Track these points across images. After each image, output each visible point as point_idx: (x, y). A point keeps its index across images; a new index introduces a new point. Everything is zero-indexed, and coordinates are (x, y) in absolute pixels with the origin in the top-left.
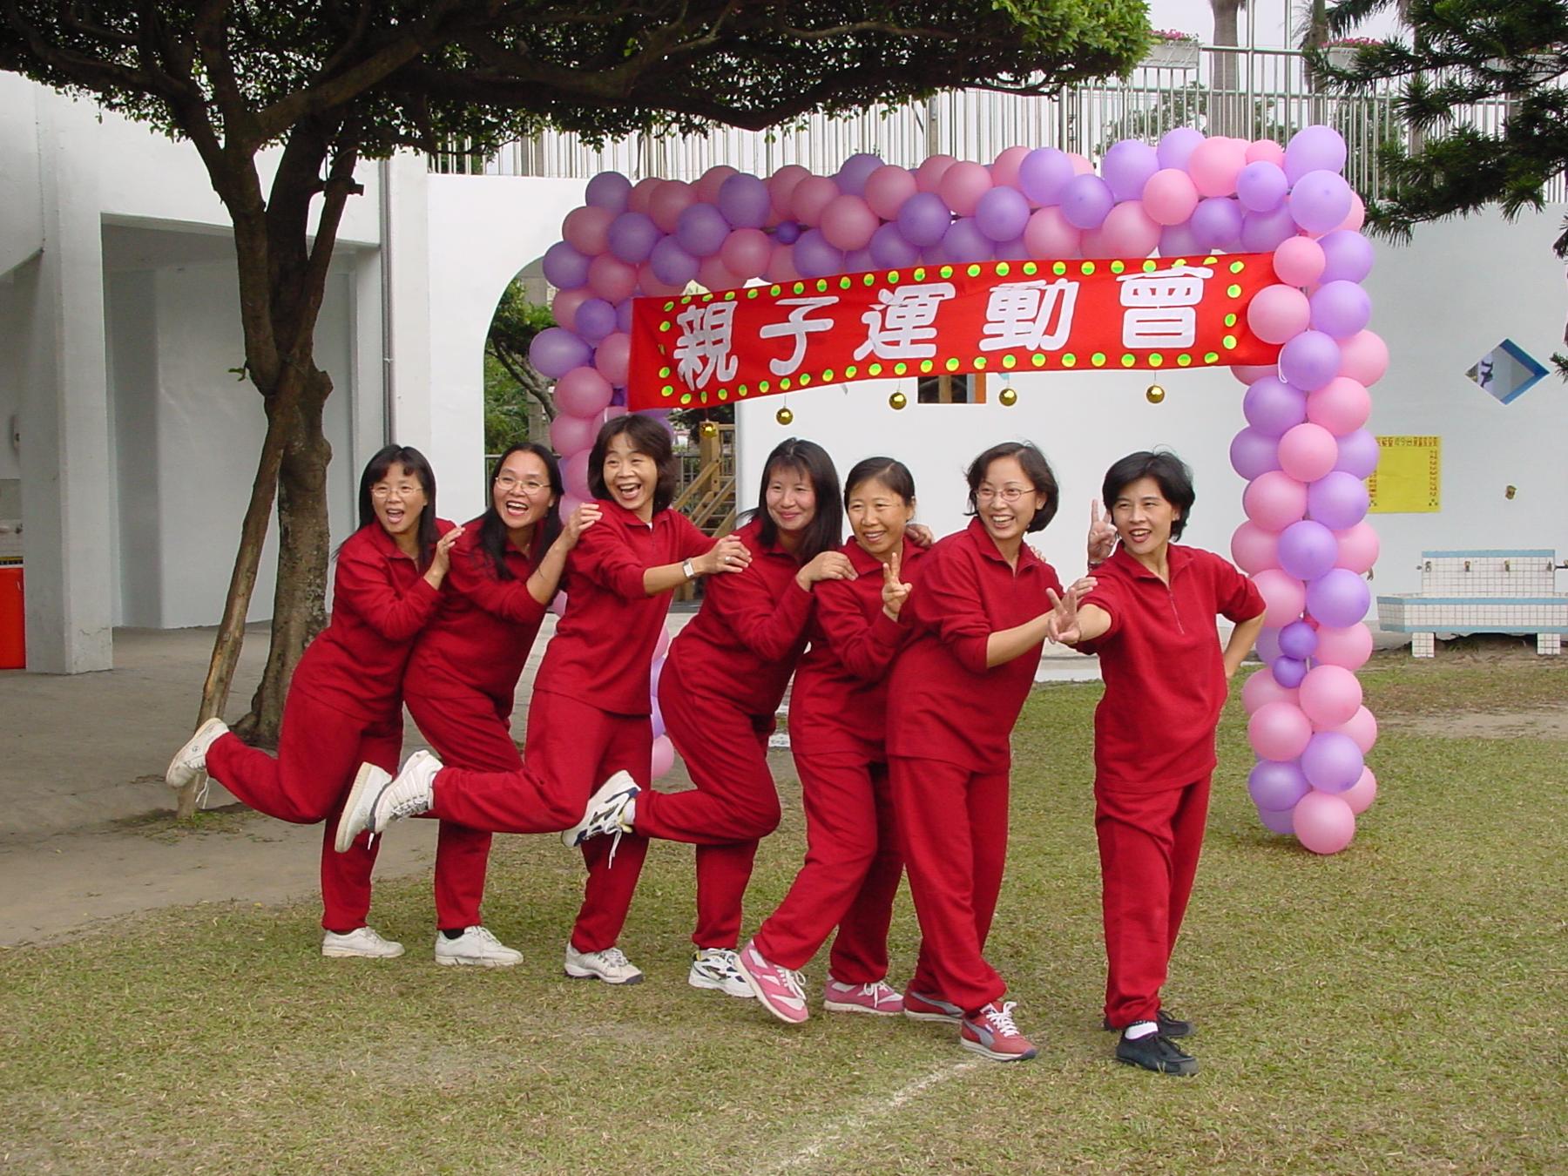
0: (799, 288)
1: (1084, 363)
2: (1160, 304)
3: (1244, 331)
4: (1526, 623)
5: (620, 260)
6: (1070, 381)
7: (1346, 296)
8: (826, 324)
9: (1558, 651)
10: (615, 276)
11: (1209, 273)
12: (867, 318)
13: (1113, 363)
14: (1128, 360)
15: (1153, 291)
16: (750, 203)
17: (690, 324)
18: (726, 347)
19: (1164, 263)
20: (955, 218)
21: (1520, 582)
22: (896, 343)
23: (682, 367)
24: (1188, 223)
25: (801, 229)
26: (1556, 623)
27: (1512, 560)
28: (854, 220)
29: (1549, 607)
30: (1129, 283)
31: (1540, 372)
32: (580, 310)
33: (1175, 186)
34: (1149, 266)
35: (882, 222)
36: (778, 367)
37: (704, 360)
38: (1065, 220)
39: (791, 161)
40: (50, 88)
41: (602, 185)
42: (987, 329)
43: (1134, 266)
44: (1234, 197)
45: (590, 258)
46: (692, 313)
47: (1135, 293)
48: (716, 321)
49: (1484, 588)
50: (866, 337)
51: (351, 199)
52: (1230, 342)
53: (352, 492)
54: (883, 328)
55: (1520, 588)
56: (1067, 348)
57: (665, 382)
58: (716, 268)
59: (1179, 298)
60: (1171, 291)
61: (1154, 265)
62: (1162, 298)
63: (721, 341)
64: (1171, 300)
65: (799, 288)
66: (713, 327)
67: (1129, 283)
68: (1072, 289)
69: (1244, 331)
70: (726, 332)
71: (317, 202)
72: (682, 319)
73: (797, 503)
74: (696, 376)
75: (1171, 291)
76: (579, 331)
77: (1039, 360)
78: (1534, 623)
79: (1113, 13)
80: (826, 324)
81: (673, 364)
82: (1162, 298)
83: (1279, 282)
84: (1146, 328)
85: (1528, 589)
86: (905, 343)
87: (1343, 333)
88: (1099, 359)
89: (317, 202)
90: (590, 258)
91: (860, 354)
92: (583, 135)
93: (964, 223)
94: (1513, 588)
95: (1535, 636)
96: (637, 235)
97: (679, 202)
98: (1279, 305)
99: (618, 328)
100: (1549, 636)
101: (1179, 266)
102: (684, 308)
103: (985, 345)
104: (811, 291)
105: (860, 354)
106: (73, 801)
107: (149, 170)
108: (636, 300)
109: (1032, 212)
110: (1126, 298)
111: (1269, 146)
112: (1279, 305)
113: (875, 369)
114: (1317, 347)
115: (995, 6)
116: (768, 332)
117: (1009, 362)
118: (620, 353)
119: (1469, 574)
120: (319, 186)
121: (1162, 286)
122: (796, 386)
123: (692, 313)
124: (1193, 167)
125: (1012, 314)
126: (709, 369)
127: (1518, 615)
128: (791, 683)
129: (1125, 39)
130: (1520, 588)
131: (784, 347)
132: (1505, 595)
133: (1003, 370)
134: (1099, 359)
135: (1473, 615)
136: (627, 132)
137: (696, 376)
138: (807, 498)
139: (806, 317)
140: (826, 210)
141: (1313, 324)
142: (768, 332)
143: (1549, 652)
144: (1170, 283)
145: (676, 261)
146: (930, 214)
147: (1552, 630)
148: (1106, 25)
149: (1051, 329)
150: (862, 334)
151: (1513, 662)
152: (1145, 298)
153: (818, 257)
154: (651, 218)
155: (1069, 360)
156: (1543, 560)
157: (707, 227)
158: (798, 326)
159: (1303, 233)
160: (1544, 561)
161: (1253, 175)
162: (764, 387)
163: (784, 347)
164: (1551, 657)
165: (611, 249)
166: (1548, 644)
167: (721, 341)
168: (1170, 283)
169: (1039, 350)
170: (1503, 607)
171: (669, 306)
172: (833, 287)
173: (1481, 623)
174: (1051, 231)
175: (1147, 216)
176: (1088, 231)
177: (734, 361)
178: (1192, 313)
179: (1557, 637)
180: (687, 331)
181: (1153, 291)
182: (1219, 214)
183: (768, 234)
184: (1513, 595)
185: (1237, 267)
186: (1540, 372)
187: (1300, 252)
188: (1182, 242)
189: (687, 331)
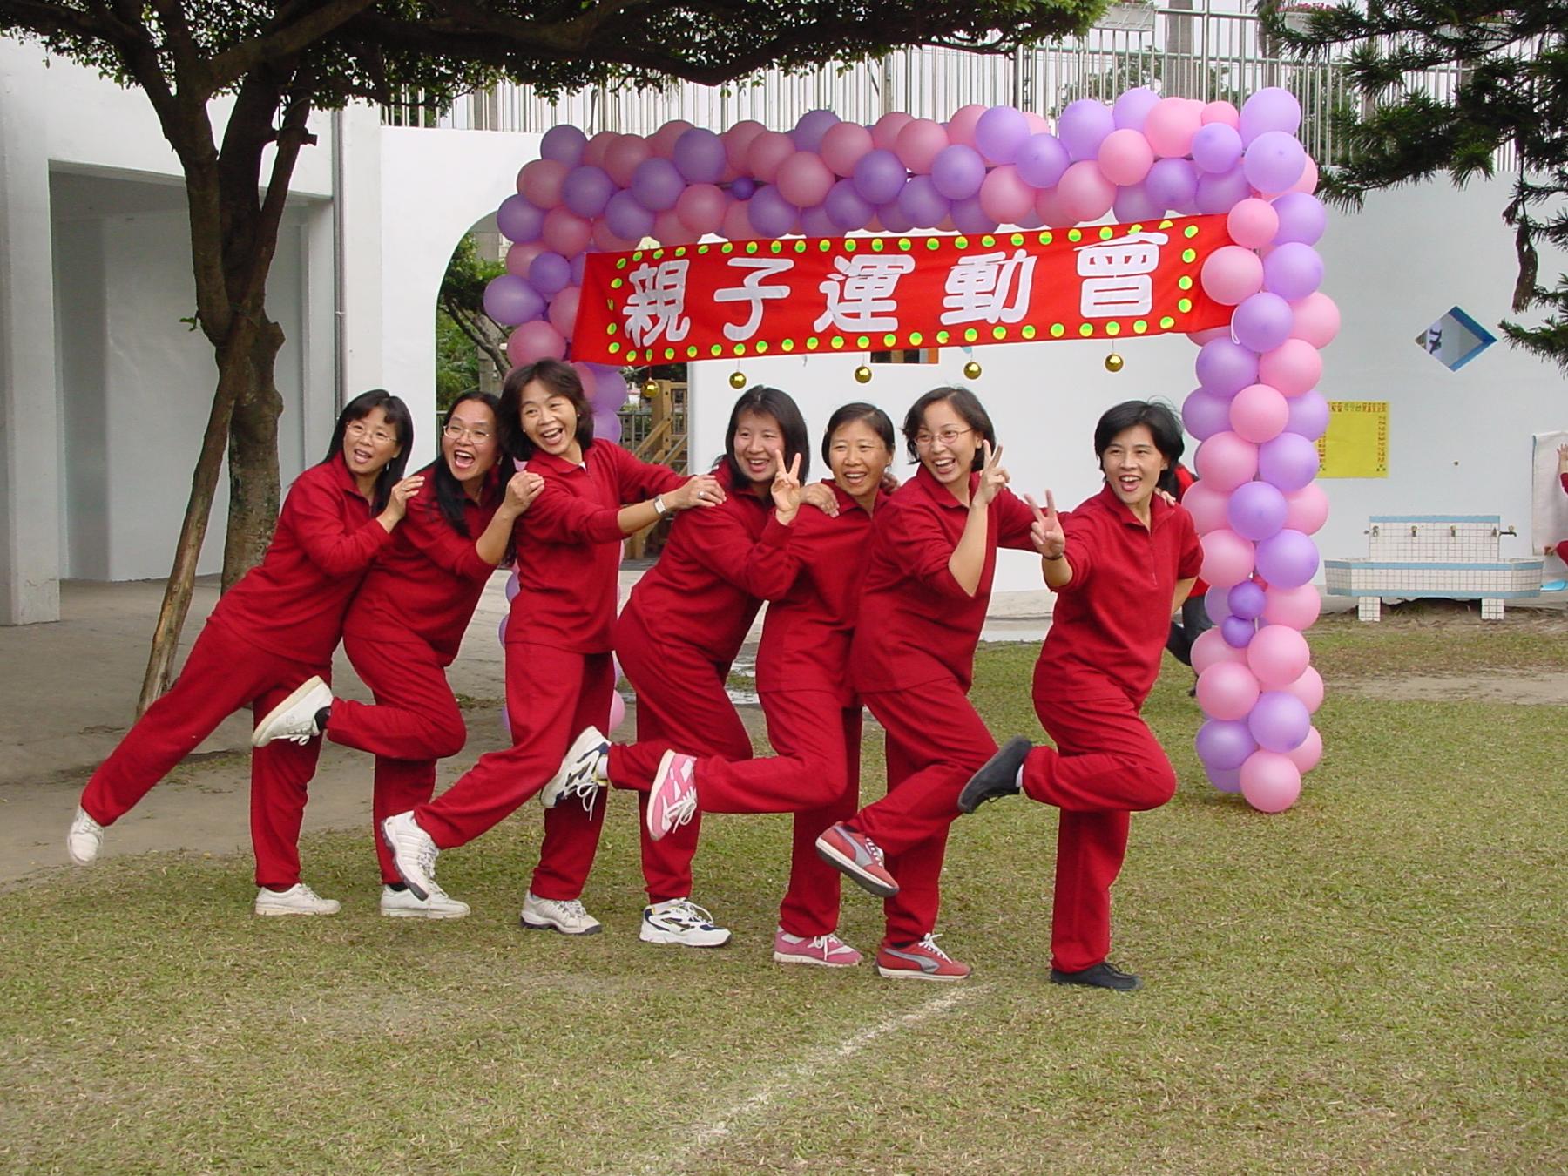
0: (752, 247)
1: (1043, 334)
2: (1118, 272)
3: (1198, 294)
7: (1299, 258)
8: (782, 292)
9: (1501, 616)
10: (569, 230)
12: (824, 287)
13: (1072, 333)
14: (1086, 330)
15: (1110, 260)
16: (706, 158)
17: (643, 282)
18: (678, 308)
19: (1120, 230)
20: (910, 175)
21: (1466, 547)
22: (856, 315)
23: (630, 324)
24: (1143, 184)
25: (756, 185)
26: (1500, 588)
27: (1458, 526)
28: (810, 177)
29: (1493, 573)
30: (1085, 253)
31: (1488, 339)
33: (1131, 147)
35: (838, 178)
36: (730, 331)
37: (655, 320)
38: (1020, 180)
42: (947, 302)
43: (1091, 236)
44: (1189, 158)
45: (545, 211)
47: (1092, 261)
48: (668, 281)
50: (825, 307)
51: (304, 149)
52: (1185, 305)
54: (842, 299)
56: (1026, 321)
58: (671, 223)
59: (1135, 266)
60: (1127, 259)
63: (673, 302)
65: (752, 247)
66: (666, 288)
67: (1085, 253)
68: (1029, 264)
69: (1198, 294)
70: (679, 293)
72: (634, 277)
74: (643, 333)
75: (1127, 259)
76: (533, 282)
77: (1000, 333)
78: (1478, 588)
80: (782, 292)
81: (621, 320)
82: (1118, 267)
83: (1232, 243)
84: (1105, 297)
85: (1473, 554)
86: (865, 316)
87: (1295, 294)
88: (716, 350)
90: (545, 211)
91: (820, 325)
92: (538, 88)
93: (920, 181)
95: (1480, 601)
96: (592, 189)
97: (635, 156)
98: (1232, 266)
99: (572, 282)
100: (1493, 602)
103: (946, 319)
104: (764, 251)
105: (820, 325)
106: (19, 751)
109: (988, 171)
110: (1083, 268)
112: (1232, 266)
113: (837, 342)
114: (1270, 308)
116: (723, 295)
117: (971, 335)
118: (569, 306)
120: (272, 136)
121: (1118, 254)
122: (751, 352)
123: (645, 272)
124: (1148, 128)
125: (970, 288)
126: (659, 328)
131: (740, 312)
132: (1451, 561)
134: (1057, 330)
136: (582, 85)
137: (643, 333)
139: (762, 282)
140: (782, 165)
141: (1266, 286)
142: (723, 295)
143: (1493, 617)
145: (630, 215)
146: (886, 172)
147: (1496, 596)
149: (1010, 302)
150: (821, 305)
151: (1457, 627)
152: (1101, 267)
153: (774, 212)
155: (1029, 332)
156: (1488, 526)
157: (663, 181)
158: (753, 291)
159: (1256, 194)
161: (1208, 137)
162: (716, 350)
163: (740, 312)
164: (1495, 622)
165: (565, 203)
166: (1492, 609)
167: (673, 302)
169: (1000, 323)
171: (621, 263)
172: (788, 250)
173: (1427, 588)
174: (1006, 189)
175: (1103, 175)
178: (1148, 280)
179: (1501, 602)
180: (639, 290)
181: (1110, 260)
182: (1174, 176)
184: (1458, 561)
185: (1191, 231)
186: (1488, 339)
187: (1254, 214)
188: (1137, 204)
189: (639, 290)
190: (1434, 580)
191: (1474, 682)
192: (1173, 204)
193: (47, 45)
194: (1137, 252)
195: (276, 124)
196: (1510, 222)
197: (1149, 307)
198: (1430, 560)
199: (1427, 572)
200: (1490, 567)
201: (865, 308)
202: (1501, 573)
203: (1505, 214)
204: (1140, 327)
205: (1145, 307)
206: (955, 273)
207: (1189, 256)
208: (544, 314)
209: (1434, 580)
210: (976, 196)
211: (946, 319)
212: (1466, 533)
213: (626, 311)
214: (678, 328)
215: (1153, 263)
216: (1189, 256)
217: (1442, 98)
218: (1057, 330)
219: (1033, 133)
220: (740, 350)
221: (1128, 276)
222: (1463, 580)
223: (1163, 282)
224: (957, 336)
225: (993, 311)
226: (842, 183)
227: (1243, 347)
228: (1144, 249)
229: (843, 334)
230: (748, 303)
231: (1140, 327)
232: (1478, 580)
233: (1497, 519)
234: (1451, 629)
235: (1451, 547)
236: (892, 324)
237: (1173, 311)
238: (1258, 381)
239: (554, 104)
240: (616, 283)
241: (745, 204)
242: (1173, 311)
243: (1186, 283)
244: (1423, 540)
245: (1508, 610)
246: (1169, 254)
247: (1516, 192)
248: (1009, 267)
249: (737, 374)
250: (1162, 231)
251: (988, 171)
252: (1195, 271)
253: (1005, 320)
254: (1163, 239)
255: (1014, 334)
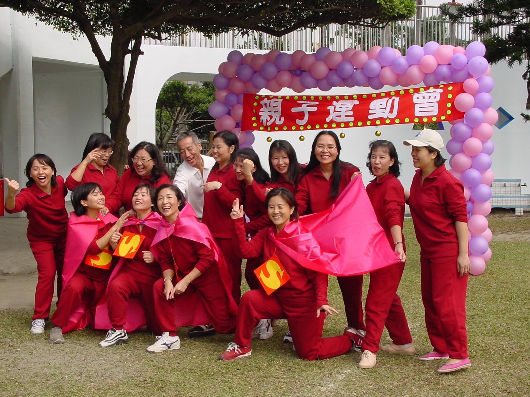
1: (402, 122)
2: (427, 102)
3: (453, 108)
4: (512, 204)
5: (239, 79)
6: (398, 127)
7: (485, 97)
8: (315, 109)
9: (522, 214)
10: (238, 86)
11: (441, 91)
12: (329, 108)
15: (424, 98)
17: (266, 104)
18: (280, 114)
19: (426, 89)
20: (355, 69)
21: (509, 190)
22: (340, 116)
23: (262, 118)
24: (435, 73)
25: (303, 71)
26: (522, 204)
27: (507, 183)
29: (520, 199)
30: (416, 96)
31: (511, 118)
32: (226, 97)
33: (431, 60)
34: (422, 90)
35: (331, 70)
36: (298, 122)
37: (271, 117)
38: (393, 71)
39: (299, 49)
40: (20, 13)
41: (231, 56)
42: (370, 112)
43: (417, 90)
44: (449, 64)
45: (230, 79)
46: (266, 101)
47: (418, 98)
49: (497, 192)
52: (449, 112)
53: (103, 109)
54: (335, 111)
55: (509, 192)
56: (397, 117)
57: (254, 122)
60: (430, 97)
61: (423, 89)
62: (427, 100)
63: (277, 111)
64: (430, 100)
66: (274, 107)
67: (416, 96)
68: (397, 100)
69: (453, 108)
70: (279, 108)
71: (128, 58)
72: (262, 102)
73: (285, 163)
74: (267, 121)
75: (430, 97)
76: (226, 102)
77: (388, 121)
78: (514, 204)
79: (406, 2)
81: (258, 117)
82: (427, 100)
83: (464, 92)
84: (422, 110)
85: (512, 192)
86: (343, 117)
87: (484, 108)
89: (128, 58)
90: (230, 79)
91: (328, 120)
92: (205, 34)
93: (359, 71)
94: (507, 192)
95: (515, 208)
96: (247, 72)
97: (261, 61)
98: (465, 99)
99: (238, 103)
100: (519, 209)
101: (432, 89)
102: (263, 99)
103: (370, 117)
105: (328, 120)
107: (72, 48)
108: (244, 94)
109: (382, 68)
110: (415, 100)
111: (460, 49)
112: (465, 99)
113: (334, 125)
114: (477, 113)
115: (378, 2)
116: (294, 110)
117: (378, 122)
118: (239, 111)
119: (492, 188)
120: (129, 52)
121: (427, 95)
122: (305, 129)
123: (266, 101)
124: (436, 54)
126: (273, 120)
127: (509, 201)
128: (123, 92)
129: (409, 10)
130: (509, 192)
131: (301, 115)
132: (504, 195)
133: (376, 125)
135: (494, 201)
136: (220, 33)
137: (267, 121)
138: (287, 161)
142: (294, 110)
143: (519, 214)
144: (429, 95)
146: (348, 68)
147: (521, 207)
148: (404, 6)
149: (391, 111)
150: (328, 113)
151: (507, 217)
152: (421, 100)
154: (251, 67)
155: (397, 121)
156: (517, 183)
157: (271, 70)
160: (518, 183)
161: (457, 58)
163: (301, 115)
164: (520, 216)
165: (238, 76)
166: (519, 212)
167: (277, 111)
168: (429, 95)
169: (388, 118)
170: (504, 199)
173: (496, 204)
174: (388, 73)
175: (420, 70)
176: (401, 77)
177: (283, 119)
178: (437, 104)
179: (522, 209)
180: (264, 107)
181: (424, 98)
182: (445, 70)
183: (291, 72)
184: (507, 195)
185: (450, 88)
186: (511, 118)
187: (471, 83)
188: (431, 79)
189: (264, 107)
190: (499, 202)
191: (520, 236)
192: (444, 79)
193: (37, 18)
194: (433, 95)
195: (130, 48)
196: (525, 79)
197: (437, 113)
198: (497, 195)
199: (497, 199)
200: (518, 197)
201: (343, 114)
202: (522, 199)
203: (523, 76)
204: (351, 124)
205: (436, 112)
206: (372, 103)
207: (450, 96)
208: (229, 113)
209: (499, 202)
210: (378, 76)
211: (370, 117)
212: (509, 185)
213: (260, 114)
214: (280, 120)
215: (438, 99)
216: (450, 96)
217: (504, 37)
218: (360, 123)
219: (397, 56)
220: (302, 128)
221: (406, 99)
222: (496, 201)
223: (442, 104)
224: (373, 123)
225: (385, 114)
226: (332, 71)
227: (467, 126)
228: (435, 94)
229: (336, 122)
230: (303, 113)
231: (351, 124)
232: (514, 202)
233: (520, 181)
234: (506, 218)
235: (504, 190)
236: (352, 119)
237: (445, 114)
238: (472, 137)
239: (211, 39)
240: (255, 104)
241: (299, 77)
242: (445, 114)
243: (449, 105)
244: (494, 188)
245: (524, 212)
246: (443, 96)
247: (527, 68)
248: (390, 101)
249: (302, 136)
250: (441, 88)
251: (382, 68)
252: (452, 101)
253: (389, 117)
254: (441, 91)
255: (392, 122)
